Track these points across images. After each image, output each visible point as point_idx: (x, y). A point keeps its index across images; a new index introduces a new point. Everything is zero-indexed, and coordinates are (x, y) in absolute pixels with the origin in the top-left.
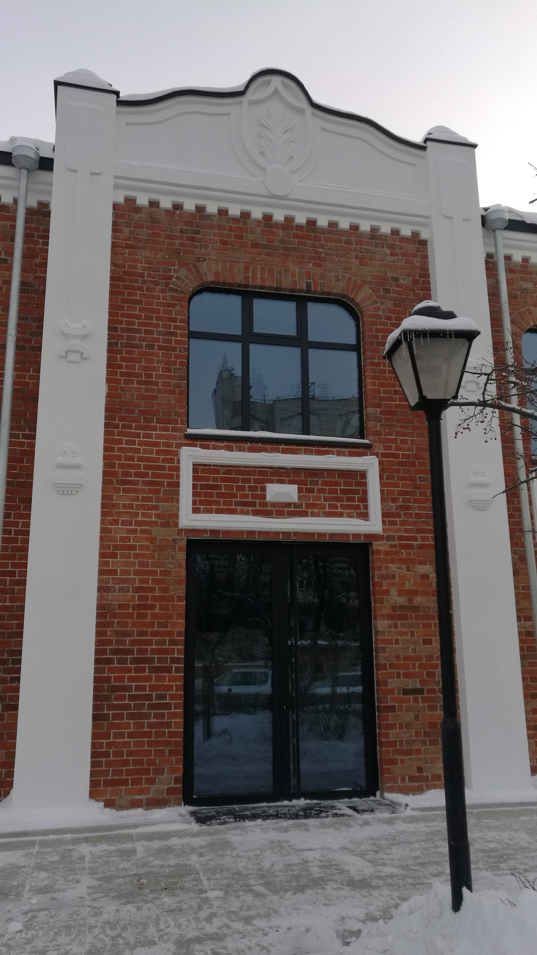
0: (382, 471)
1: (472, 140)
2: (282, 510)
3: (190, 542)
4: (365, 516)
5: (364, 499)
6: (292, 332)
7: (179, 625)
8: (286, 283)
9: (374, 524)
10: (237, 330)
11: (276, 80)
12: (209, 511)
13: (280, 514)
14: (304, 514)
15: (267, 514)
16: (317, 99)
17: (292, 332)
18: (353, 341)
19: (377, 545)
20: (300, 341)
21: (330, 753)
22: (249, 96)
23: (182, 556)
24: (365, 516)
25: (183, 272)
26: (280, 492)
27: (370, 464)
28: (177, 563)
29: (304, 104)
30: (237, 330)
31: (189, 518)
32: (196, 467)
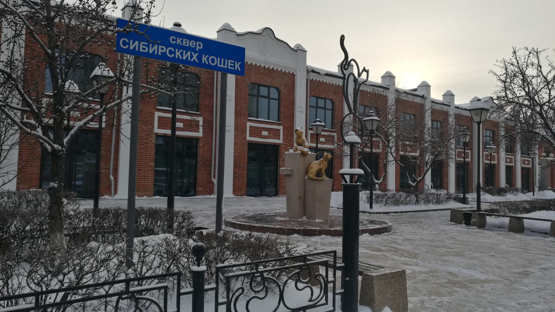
0: (203, 121)
1: (306, 50)
2: (265, 137)
3: (248, 143)
4: (279, 139)
5: (279, 136)
6: (267, 95)
7: (246, 161)
8: (267, 84)
9: (281, 141)
10: (315, 105)
11: (268, 30)
12: (162, 128)
13: (264, 138)
14: (185, 131)
15: (262, 138)
16: (277, 36)
17: (267, 95)
18: (277, 98)
19: (282, 146)
20: (268, 97)
21: (193, 192)
22: (263, 34)
23: (247, 146)
24: (279, 139)
25: (248, 80)
26: (265, 133)
27: (281, 128)
28: (246, 148)
29: (273, 37)
30: (315, 105)
31: (249, 138)
32: (159, 117)
